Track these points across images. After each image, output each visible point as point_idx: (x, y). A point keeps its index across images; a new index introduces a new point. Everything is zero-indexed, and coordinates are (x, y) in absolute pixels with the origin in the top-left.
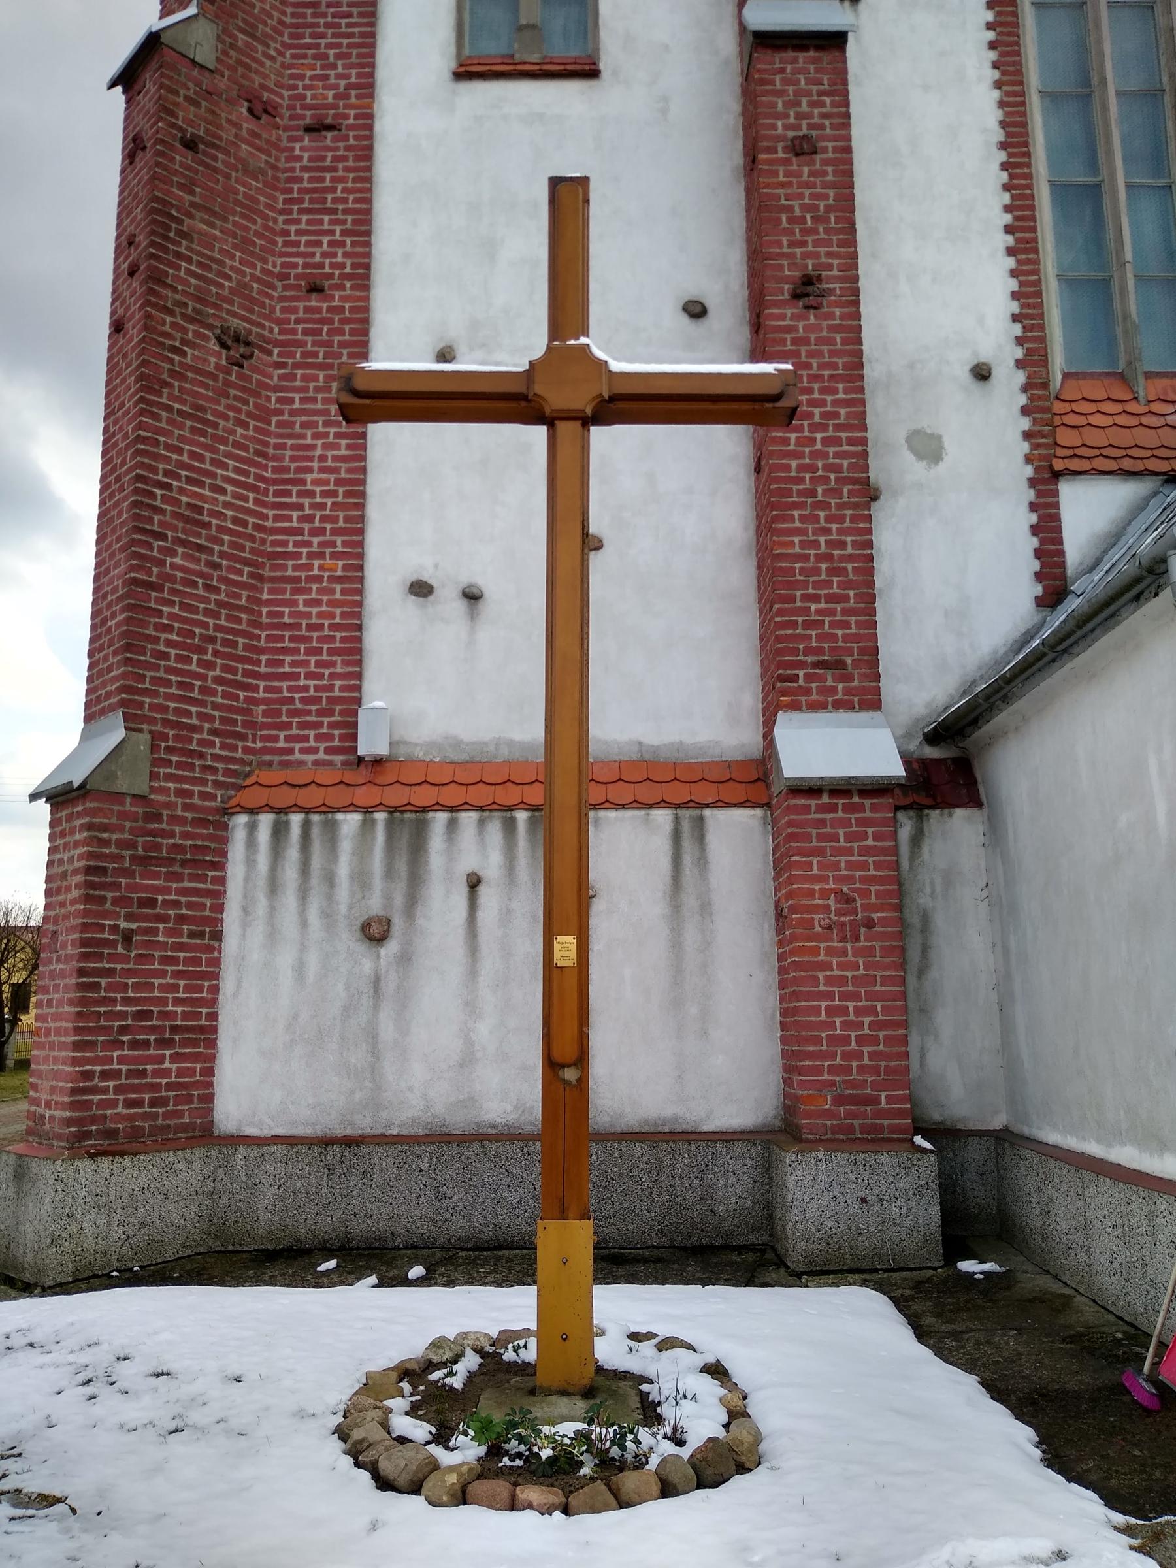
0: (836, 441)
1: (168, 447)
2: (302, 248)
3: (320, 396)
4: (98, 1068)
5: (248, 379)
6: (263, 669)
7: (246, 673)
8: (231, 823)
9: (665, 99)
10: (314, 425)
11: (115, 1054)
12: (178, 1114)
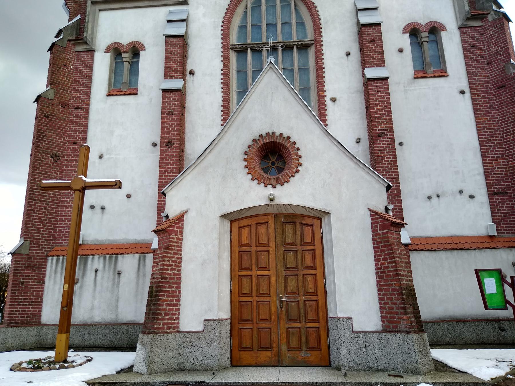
1: (37, 181)
2: (73, 135)
3: (74, 166)
4: (15, 310)
5: (59, 164)
6: (58, 225)
7: (54, 227)
8: (48, 259)
9: (151, 99)
10: (488, 121)
11: (19, 307)
12: (33, 319)
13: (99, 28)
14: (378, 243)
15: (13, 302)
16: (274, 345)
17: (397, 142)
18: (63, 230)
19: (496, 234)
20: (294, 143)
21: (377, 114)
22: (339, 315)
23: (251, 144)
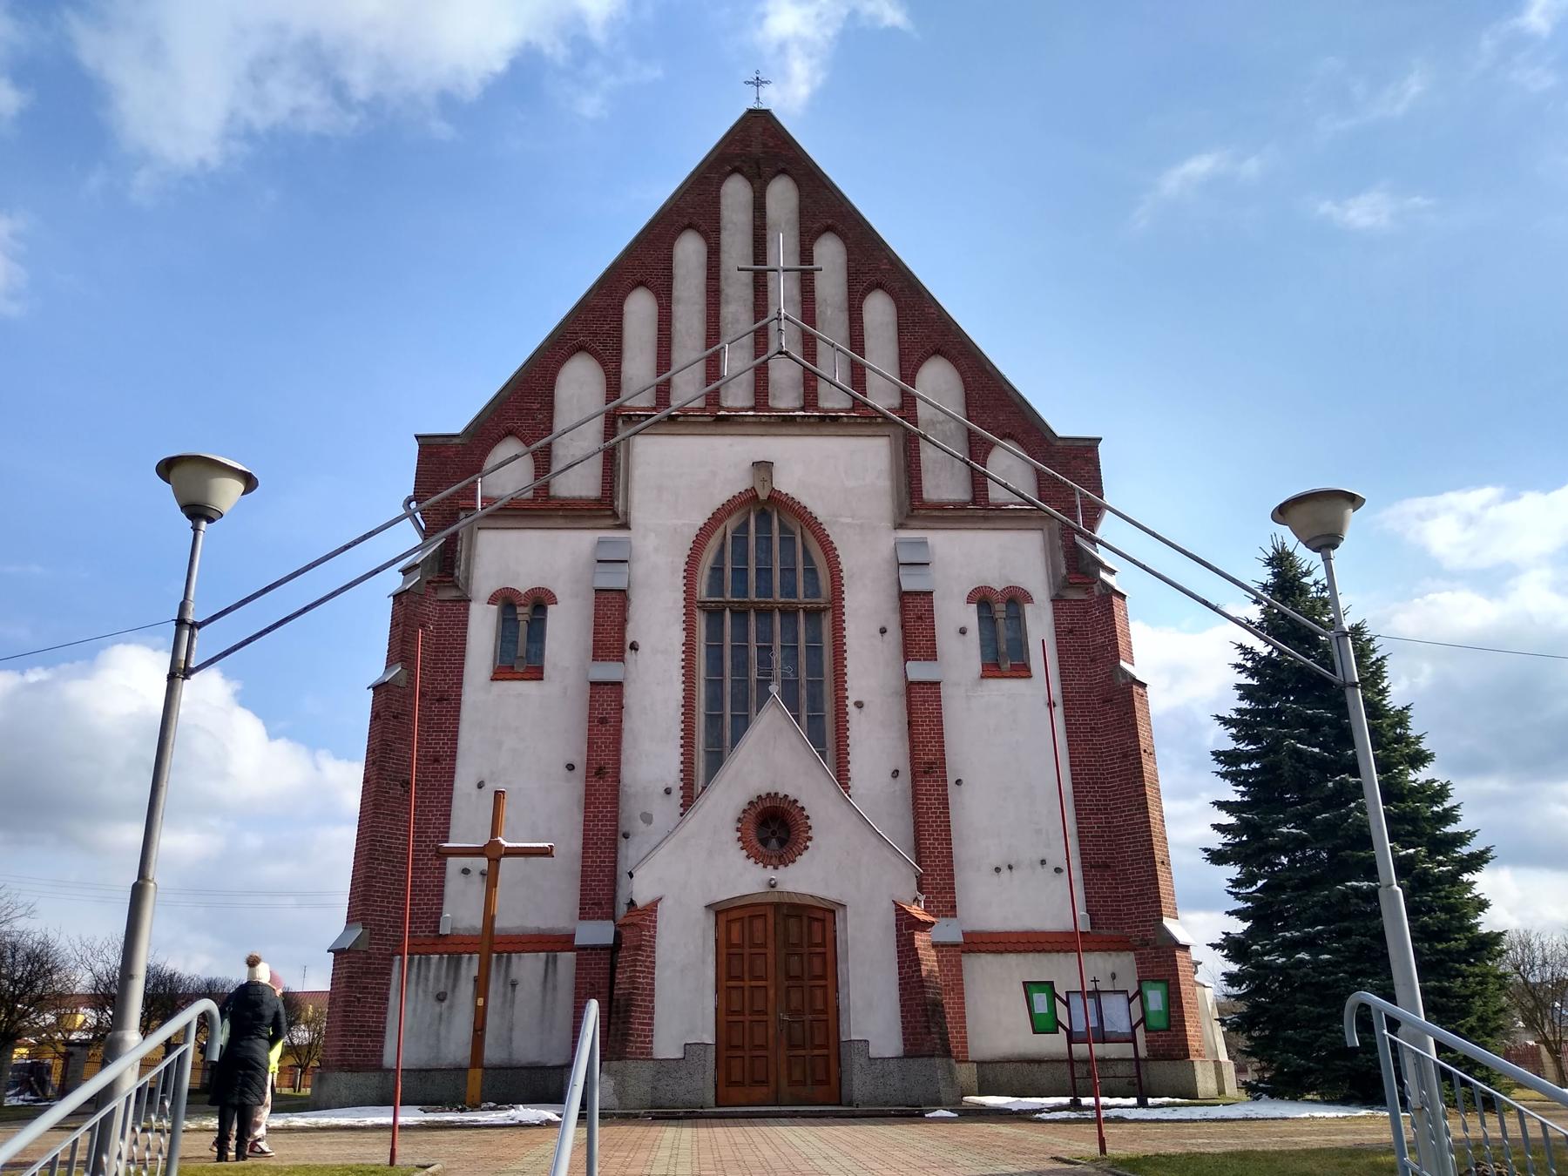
0: (606, 825)
10: (432, 811)
13: (477, 559)
14: (903, 946)
15: (345, 1031)
16: (772, 1079)
17: (951, 780)
18: (417, 909)
19: (1089, 930)
20: (803, 809)
21: (923, 738)
22: (853, 1038)
23: (746, 808)
